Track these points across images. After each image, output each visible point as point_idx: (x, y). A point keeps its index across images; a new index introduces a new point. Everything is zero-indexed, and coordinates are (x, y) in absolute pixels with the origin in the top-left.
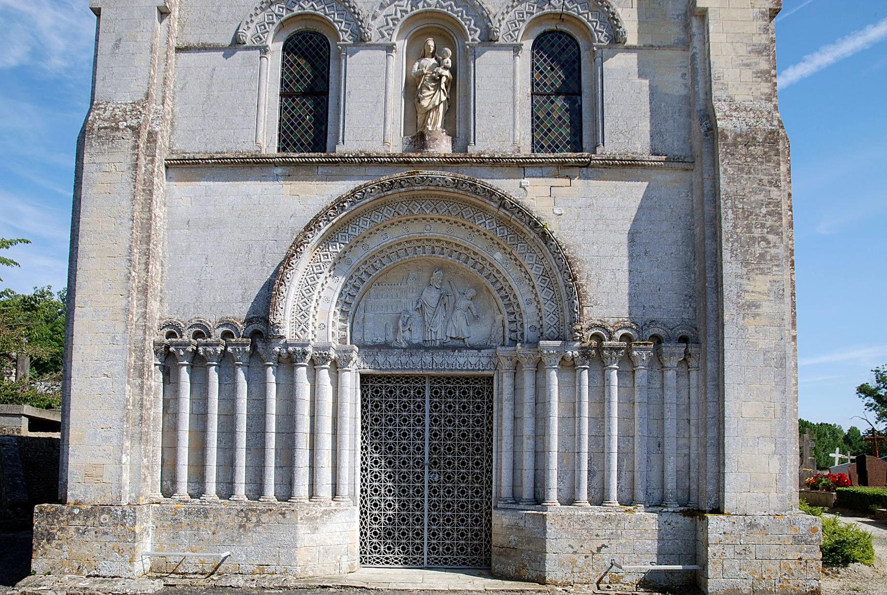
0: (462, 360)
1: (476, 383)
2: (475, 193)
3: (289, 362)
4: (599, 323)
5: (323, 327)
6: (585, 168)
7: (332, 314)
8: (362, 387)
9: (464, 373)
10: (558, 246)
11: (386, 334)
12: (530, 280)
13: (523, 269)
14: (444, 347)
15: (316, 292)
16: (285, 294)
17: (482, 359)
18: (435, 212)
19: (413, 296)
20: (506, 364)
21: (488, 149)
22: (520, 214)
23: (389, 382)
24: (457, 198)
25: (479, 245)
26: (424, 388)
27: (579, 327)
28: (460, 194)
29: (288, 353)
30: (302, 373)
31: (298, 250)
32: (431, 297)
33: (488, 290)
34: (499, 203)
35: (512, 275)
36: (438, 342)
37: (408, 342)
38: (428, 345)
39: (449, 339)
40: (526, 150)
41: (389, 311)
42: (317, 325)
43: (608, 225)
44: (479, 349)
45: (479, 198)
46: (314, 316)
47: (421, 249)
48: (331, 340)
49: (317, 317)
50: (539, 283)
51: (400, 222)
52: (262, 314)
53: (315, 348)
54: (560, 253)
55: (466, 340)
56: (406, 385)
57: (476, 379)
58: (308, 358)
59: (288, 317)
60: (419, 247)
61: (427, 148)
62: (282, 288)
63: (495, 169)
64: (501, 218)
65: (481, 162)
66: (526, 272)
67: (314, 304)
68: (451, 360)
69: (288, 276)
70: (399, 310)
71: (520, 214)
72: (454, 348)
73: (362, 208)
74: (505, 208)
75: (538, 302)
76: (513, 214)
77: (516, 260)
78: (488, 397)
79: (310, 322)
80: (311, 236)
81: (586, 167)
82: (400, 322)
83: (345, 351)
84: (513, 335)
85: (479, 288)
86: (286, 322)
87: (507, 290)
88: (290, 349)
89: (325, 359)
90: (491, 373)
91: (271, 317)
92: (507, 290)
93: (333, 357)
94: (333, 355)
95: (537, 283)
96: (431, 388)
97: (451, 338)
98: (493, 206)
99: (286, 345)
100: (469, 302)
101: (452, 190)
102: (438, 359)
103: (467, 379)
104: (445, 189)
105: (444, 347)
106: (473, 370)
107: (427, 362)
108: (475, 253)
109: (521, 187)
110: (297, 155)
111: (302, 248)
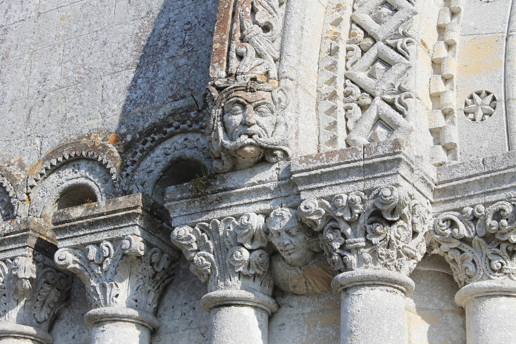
29: (306, 228)
42: (454, 100)
46: (437, 65)
49: (451, 68)
88: (312, 202)
99: (290, 187)
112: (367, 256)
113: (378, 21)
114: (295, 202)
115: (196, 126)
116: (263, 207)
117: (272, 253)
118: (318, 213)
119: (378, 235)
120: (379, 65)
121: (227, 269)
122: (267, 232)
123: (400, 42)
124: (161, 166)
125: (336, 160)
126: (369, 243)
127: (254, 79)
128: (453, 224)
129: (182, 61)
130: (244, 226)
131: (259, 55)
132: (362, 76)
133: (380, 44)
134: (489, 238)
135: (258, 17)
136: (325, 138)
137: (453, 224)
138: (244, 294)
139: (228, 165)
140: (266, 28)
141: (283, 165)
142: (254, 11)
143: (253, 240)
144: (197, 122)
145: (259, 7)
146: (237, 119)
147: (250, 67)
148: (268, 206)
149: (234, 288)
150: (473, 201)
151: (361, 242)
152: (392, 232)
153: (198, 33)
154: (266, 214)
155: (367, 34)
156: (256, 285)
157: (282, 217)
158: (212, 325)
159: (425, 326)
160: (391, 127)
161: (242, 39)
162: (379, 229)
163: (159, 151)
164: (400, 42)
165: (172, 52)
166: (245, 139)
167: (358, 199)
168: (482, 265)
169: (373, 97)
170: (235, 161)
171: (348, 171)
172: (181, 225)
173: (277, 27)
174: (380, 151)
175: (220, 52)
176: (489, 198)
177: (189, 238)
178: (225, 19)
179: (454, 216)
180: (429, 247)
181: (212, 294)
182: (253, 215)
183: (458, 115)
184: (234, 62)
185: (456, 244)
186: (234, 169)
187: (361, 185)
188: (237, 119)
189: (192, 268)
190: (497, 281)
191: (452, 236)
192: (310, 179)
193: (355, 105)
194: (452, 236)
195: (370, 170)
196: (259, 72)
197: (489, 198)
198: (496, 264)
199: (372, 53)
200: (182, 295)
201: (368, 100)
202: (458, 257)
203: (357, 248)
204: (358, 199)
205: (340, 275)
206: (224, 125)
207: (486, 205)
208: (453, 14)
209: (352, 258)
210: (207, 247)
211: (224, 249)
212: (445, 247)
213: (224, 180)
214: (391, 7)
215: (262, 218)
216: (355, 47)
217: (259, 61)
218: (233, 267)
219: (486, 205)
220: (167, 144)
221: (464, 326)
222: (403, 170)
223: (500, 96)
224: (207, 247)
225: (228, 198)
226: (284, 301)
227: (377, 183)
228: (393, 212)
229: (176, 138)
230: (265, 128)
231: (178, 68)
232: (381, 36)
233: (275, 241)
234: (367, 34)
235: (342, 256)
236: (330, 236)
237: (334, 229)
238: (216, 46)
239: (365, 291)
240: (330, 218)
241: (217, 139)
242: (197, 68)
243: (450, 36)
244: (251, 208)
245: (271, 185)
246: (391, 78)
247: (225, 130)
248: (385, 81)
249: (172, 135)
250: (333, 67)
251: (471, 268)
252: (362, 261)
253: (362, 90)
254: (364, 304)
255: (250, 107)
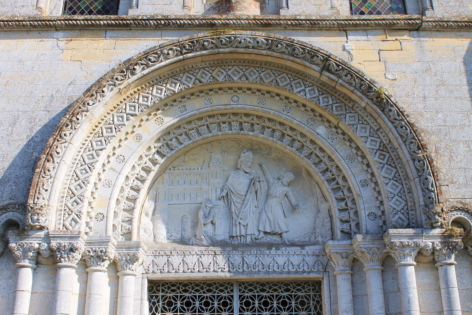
0: (281, 260)
1: (299, 290)
2: (292, 55)
3: (49, 261)
4: (459, 206)
5: (102, 217)
6: (415, 28)
7: (113, 202)
8: (150, 298)
9: (284, 276)
10: (401, 112)
11: (183, 230)
12: (364, 157)
13: (353, 145)
14: (256, 244)
15: (95, 172)
16: (53, 173)
17: (307, 259)
18: (244, 79)
19: (218, 182)
20: (339, 265)
21: (303, 12)
22: (349, 76)
23: (186, 291)
24: (269, 64)
25: (296, 119)
26: (231, 298)
27: (439, 210)
28: (272, 57)
29: (51, 250)
30: (69, 278)
31: (74, 119)
32: (239, 183)
33: (309, 174)
34: (321, 66)
35: (340, 153)
36: (249, 239)
37: (211, 238)
38: (236, 242)
39: (262, 235)
40: (344, 12)
41: (187, 201)
42: (93, 214)
43: (451, 92)
44: (302, 246)
45: (298, 60)
46: (90, 203)
47: (226, 125)
48: (110, 232)
49: (94, 205)
50: (376, 159)
51: (202, 92)
52: (22, 200)
53: (89, 243)
54: (402, 120)
55: (284, 235)
56: (209, 294)
57: (300, 284)
58: (77, 256)
59: (55, 203)
60: (224, 123)
61: (233, 10)
62: (49, 165)
63: (313, 32)
64: (324, 84)
65: (296, 25)
66: (358, 148)
67: (90, 187)
68: (267, 260)
69: (59, 150)
70: (199, 200)
71: (349, 76)
72: (270, 246)
73: (157, 73)
74: (329, 71)
75: (376, 183)
76: (340, 77)
77: (344, 134)
78: (315, 308)
79: (84, 211)
80: (91, 103)
81: (417, 30)
82: (201, 214)
83: (129, 248)
84: (346, 226)
85: (298, 172)
86: (51, 208)
87: (334, 171)
88: (54, 244)
89: (100, 258)
90: (320, 276)
91: (30, 201)
92: (334, 171)
93: (112, 257)
94: (112, 253)
95: (373, 159)
96: (241, 298)
97: (265, 233)
98: (314, 70)
99: (48, 238)
100: (286, 189)
101: (264, 52)
102: (250, 259)
103: (287, 285)
104: (256, 51)
105: (256, 244)
106: (297, 272)
107: (236, 263)
108: (292, 129)
109: (344, 49)
110: (82, 17)
111: (79, 117)
112: (67, 260)
113: (76, 189)
114: (49, 242)
115: (17, 211)
116: (39, 242)
117: (39, 253)
118: (55, 247)
119: (71, 255)
120: (75, 203)
121: (25, 257)
122: (39, 249)
123: (82, 198)
124: (4, 220)
125: (62, 233)
126: (68, 256)
127: (42, 206)
128: (89, 252)
129: (14, 188)
130: (32, 247)
131: (43, 199)
132: (70, 205)
133: (76, 197)
134: (98, 257)
135: (44, 187)
136: (58, 223)
137: (89, 252)
138: (29, 265)
139: (30, 228)
140: (46, 190)
141: (46, 231)
142: (43, 185)
143: (34, 250)
144: (18, 210)
145: (45, 184)
146: (36, 217)
147: (41, 202)
148: (40, 242)
149: (26, 263)
150: (95, 247)
151: (66, 256)
152: (74, 254)
153: (20, 180)
154: (39, 244)
155: (72, 193)
156: (33, 262)
157: (44, 246)
158: (18, 272)
159: (77, 276)
160: (76, 222)
161: (39, 193)
162: (71, 253)
163: (4, 215)
164: (82, 198)
165: (10, 184)
166: (37, 224)
167: (67, 245)
168: (95, 263)
169: (72, 212)
170: (33, 228)
171: (65, 237)
172: (13, 243)
173: (49, 190)
174: (75, 233)
175: (32, 196)
176: (100, 247)
177: (15, 247)
178: (34, 186)
179: (90, 250)
180: (82, 257)
181: (20, 264)
182: (36, 244)
183: (94, 218)
184: (36, 200)
185: (89, 257)
186: (31, 230)
187: (68, 241)
188: (36, 217)
189: (14, 255)
190: (98, 268)
191: (89, 255)
192: (54, 237)
193: (66, 213)
194: (89, 255)
195: (71, 238)
196: (43, 204)
197: (100, 247)
198: (99, 263)
199: (73, 199)
200: (6, 259)
201: (71, 213)
202: (89, 260)
203: (65, 257)
204: (67, 245)
205: (59, 264)
206: (31, 218)
207: (99, 248)
208: (96, 189)
209: (62, 260)
210: (20, 250)
211: (25, 251)
212: (86, 257)
213: (28, 232)
214: (80, 186)
215: (38, 245)
216: (69, 196)
217: (43, 200)
218: (27, 257)
219: (99, 248)
220: (7, 214)
221: (87, 277)
222: (80, 239)
223: (105, 216)
224: (20, 250)
225: (28, 238)
226: (39, 265)
227: (72, 242)
228: (76, 250)
229: (10, 213)
230: (42, 221)
231: (12, 189)
232: (76, 195)
233: (41, 252)
234: (72, 193)
235: (60, 259)
236: (58, 253)
237: (59, 251)
238: (31, 193)
239: (65, 269)
240: (58, 248)
241: (29, 222)
242: (19, 191)
243: (95, 196)
244: (35, 242)
245: (42, 236)
246: (78, 207)
247: (31, 219)
248: (76, 209)
249: (9, 211)
250: (62, 202)
251: (92, 263)
252: (65, 261)
253: (69, 209)
254: (64, 272)
255: (40, 215)
